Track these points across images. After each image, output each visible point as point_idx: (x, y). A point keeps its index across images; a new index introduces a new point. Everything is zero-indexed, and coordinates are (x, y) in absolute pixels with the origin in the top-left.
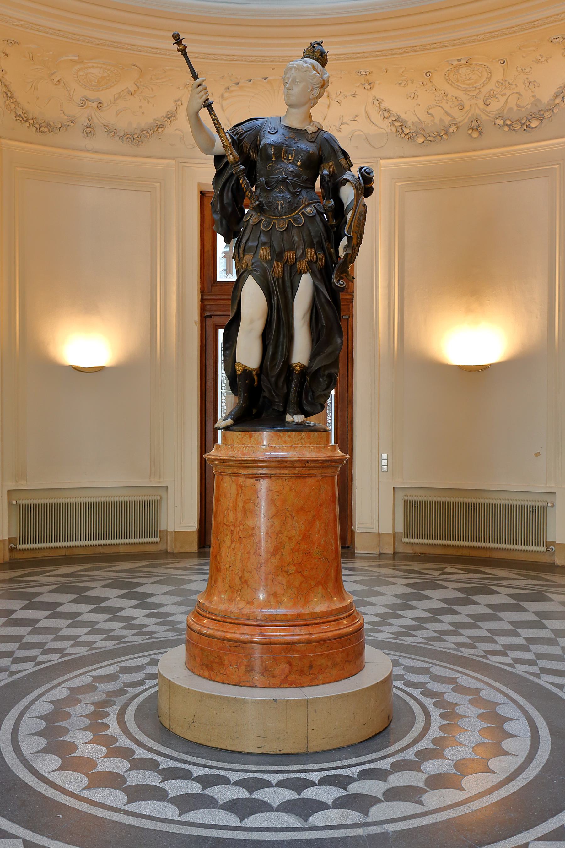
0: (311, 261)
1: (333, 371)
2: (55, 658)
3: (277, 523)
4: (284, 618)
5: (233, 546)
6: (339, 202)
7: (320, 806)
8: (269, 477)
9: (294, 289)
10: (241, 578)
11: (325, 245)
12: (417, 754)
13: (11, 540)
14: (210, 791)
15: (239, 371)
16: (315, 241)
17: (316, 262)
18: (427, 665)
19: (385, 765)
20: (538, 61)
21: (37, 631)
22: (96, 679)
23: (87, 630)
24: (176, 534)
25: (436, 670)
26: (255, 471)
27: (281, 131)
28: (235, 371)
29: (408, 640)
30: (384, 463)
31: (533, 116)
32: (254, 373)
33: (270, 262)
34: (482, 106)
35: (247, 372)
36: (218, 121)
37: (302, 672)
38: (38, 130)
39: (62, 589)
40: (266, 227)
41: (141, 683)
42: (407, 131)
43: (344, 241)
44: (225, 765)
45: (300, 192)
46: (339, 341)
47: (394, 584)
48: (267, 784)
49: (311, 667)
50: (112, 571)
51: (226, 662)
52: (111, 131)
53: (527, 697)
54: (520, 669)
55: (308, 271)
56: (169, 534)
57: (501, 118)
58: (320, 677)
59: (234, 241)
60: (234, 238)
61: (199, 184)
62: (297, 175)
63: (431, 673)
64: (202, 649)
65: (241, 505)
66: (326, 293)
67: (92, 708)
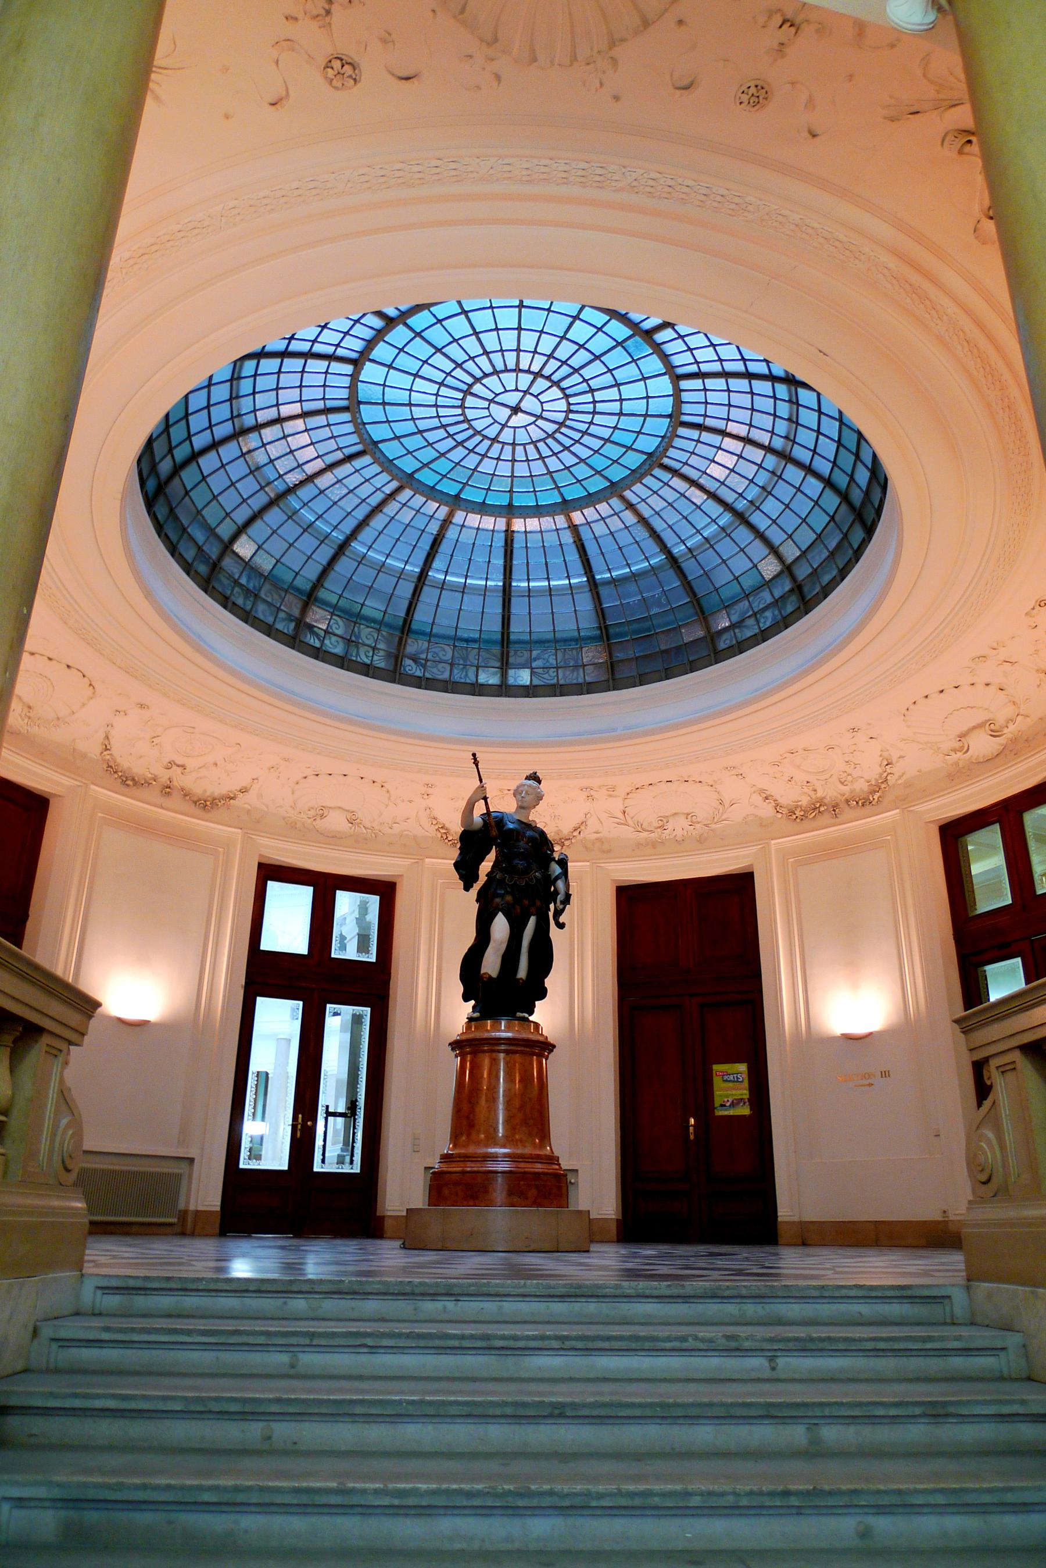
38: (124, 783)
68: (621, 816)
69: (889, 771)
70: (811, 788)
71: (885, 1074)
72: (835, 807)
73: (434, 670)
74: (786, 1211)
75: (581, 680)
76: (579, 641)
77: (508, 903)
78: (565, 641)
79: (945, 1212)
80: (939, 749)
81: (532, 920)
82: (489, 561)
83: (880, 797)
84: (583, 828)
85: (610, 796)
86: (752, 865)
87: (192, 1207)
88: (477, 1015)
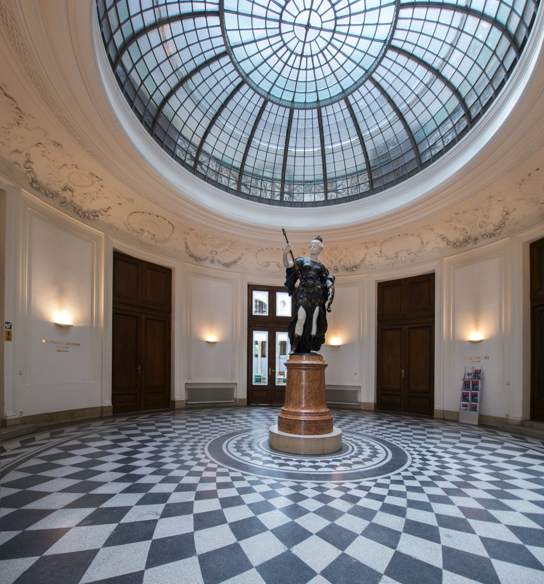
3: (310, 384)
4: (314, 413)
13: (186, 401)
20: (357, 250)
25: (355, 437)
27: (309, 262)
33: (307, 302)
34: (338, 262)
37: (320, 430)
38: (196, 260)
44: (336, 456)
48: (318, 462)
49: (322, 428)
52: (219, 262)
61: (248, 282)
62: (315, 276)
64: (287, 424)
68: (379, 253)
69: (506, 218)
70: (465, 231)
71: (487, 358)
72: (476, 239)
73: (298, 198)
74: (438, 406)
75: (358, 193)
76: (357, 173)
77: (305, 302)
78: (351, 174)
79: (507, 415)
80: (538, 201)
81: (317, 309)
82: (313, 137)
83: (500, 232)
84: (364, 260)
85: (375, 245)
86: (434, 270)
87: (238, 398)
88: (293, 352)
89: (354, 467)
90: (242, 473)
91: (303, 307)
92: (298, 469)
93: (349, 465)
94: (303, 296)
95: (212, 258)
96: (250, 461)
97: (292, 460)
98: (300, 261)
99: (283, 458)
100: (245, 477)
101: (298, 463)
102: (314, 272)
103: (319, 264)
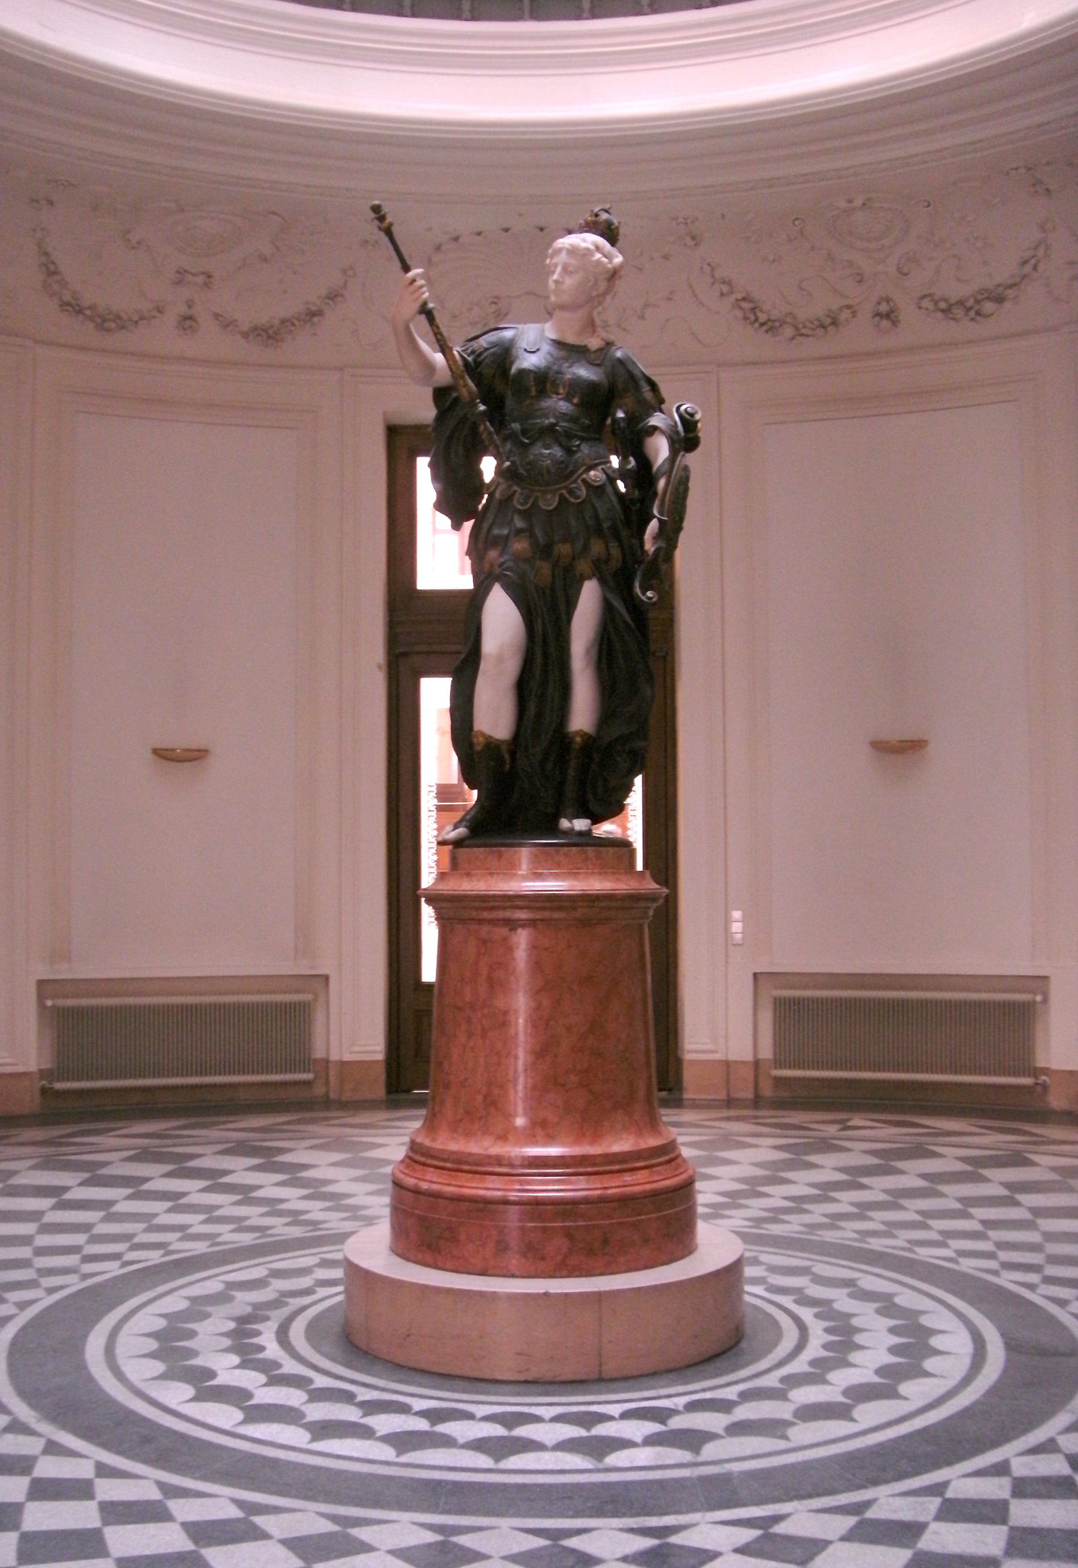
0: (599, 560)
1: (639, 744)
2: (155, 1257)
3: (546, 1003)
5: (472, 1044)
6: (645, 463)
7: (622, 1444)
8: (531, 923)
9: (571, 604)
10: (485, 1097)
11: (624, 533)
12: (783, 1380)
14: (443, 1428)
15: (479, 744)
16: (605, 525)
17: (607, 561)
18: (808, 1263)
19: (730, 1393)
21: (111, 1218)
22: (232, 1286)
23: (202, 1217)
24: (343, 1064)
25: (821, 1269)
26: (508, 914)
28: (471, 745)
29: (775, 1229)
30: (737, 927)
31: (986, 295)
32: (504, 748)
35: (492, 746)
36: (441, 335)
37: (590, 1252)
39: (144, 1156)
40: (522, 504)
41: (308, 1292)
42: (763, 317)
43: (653, 526)
44: (465, 1397)
45: (578, 446)
46: (649, 692)
47: (756, 1146)
48: (537, 1419)
49: (605, 1242)
50: (234, 1130)
51: (463, 1237)
52: (227, 324)
53: (962, 1296)
54: (967, 1265)
55: (594, 575)
56: (331, 1065)
57: (929, 299)
58: (622, 1259)
59: (468, 525)
60: (468, 519)
62: (572, 419)
63: (814, 1274)
65: (484, 972)
66: (623, 611)
67: (232, 1325)
77: (517, 558)
87: (334, 1056)
89: (803, 1433)
90: (240, 1503)
91: (509, 589)
92: (497, 1460)
93: (773, 1427)
94: (506, 532)
95: (183, 309)
96: (243, 1430)
97: (470, 1416)
98: (494, 345)
99: (419, 1405)
100: (259, 1520)
101: (498, 1430)
102: (568, 398)
103: (598, 357)
